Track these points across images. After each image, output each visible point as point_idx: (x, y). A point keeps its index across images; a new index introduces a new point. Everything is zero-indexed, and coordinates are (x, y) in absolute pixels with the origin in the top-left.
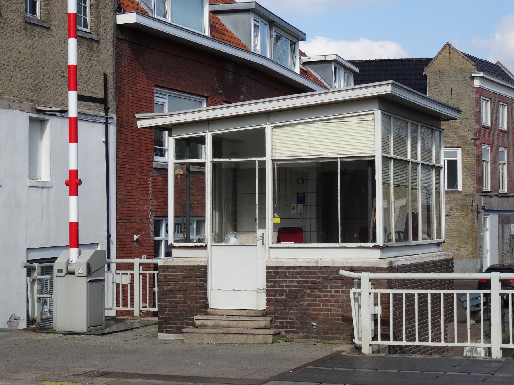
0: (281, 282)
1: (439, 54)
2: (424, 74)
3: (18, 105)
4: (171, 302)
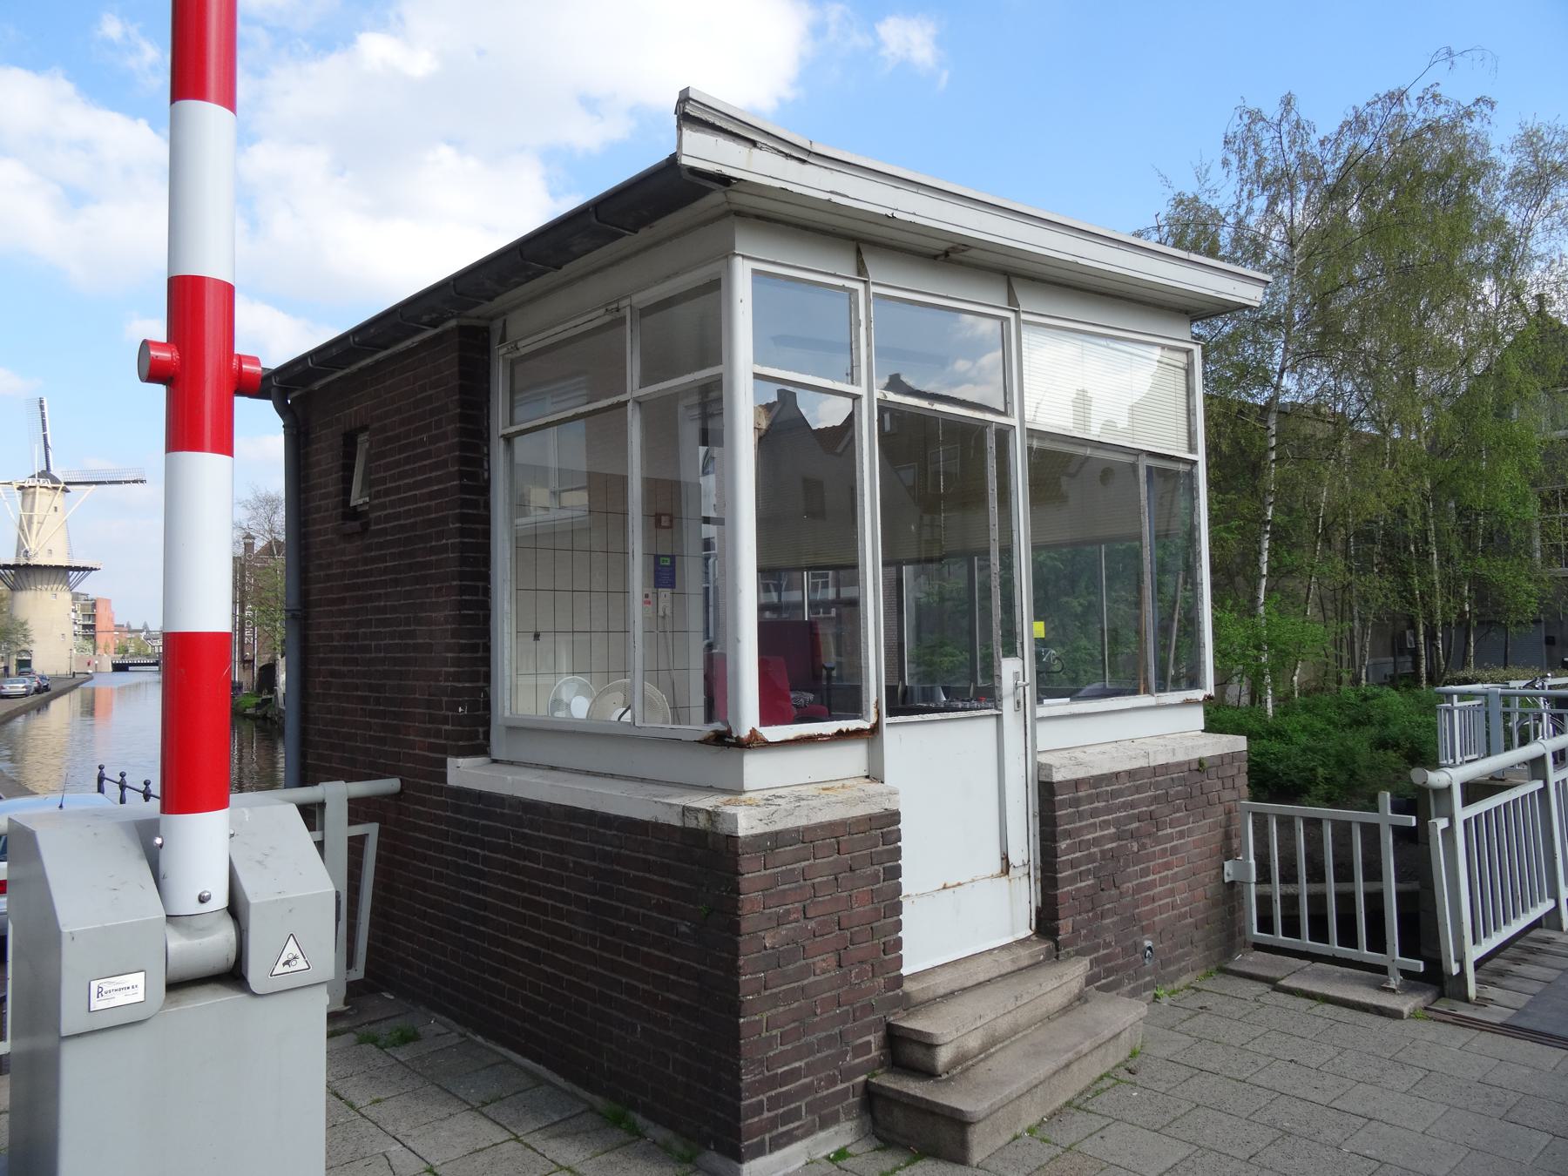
0: (1085, 832)
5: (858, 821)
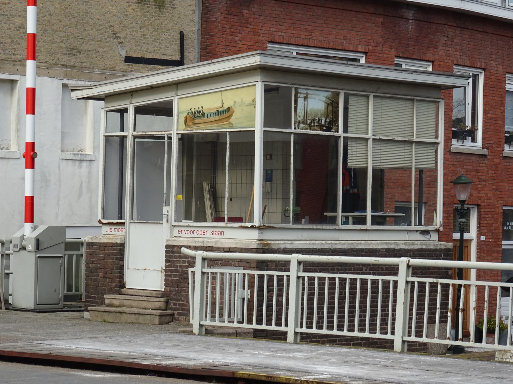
0: (176, 262)
3: (47, 71)
5: (110, 243)
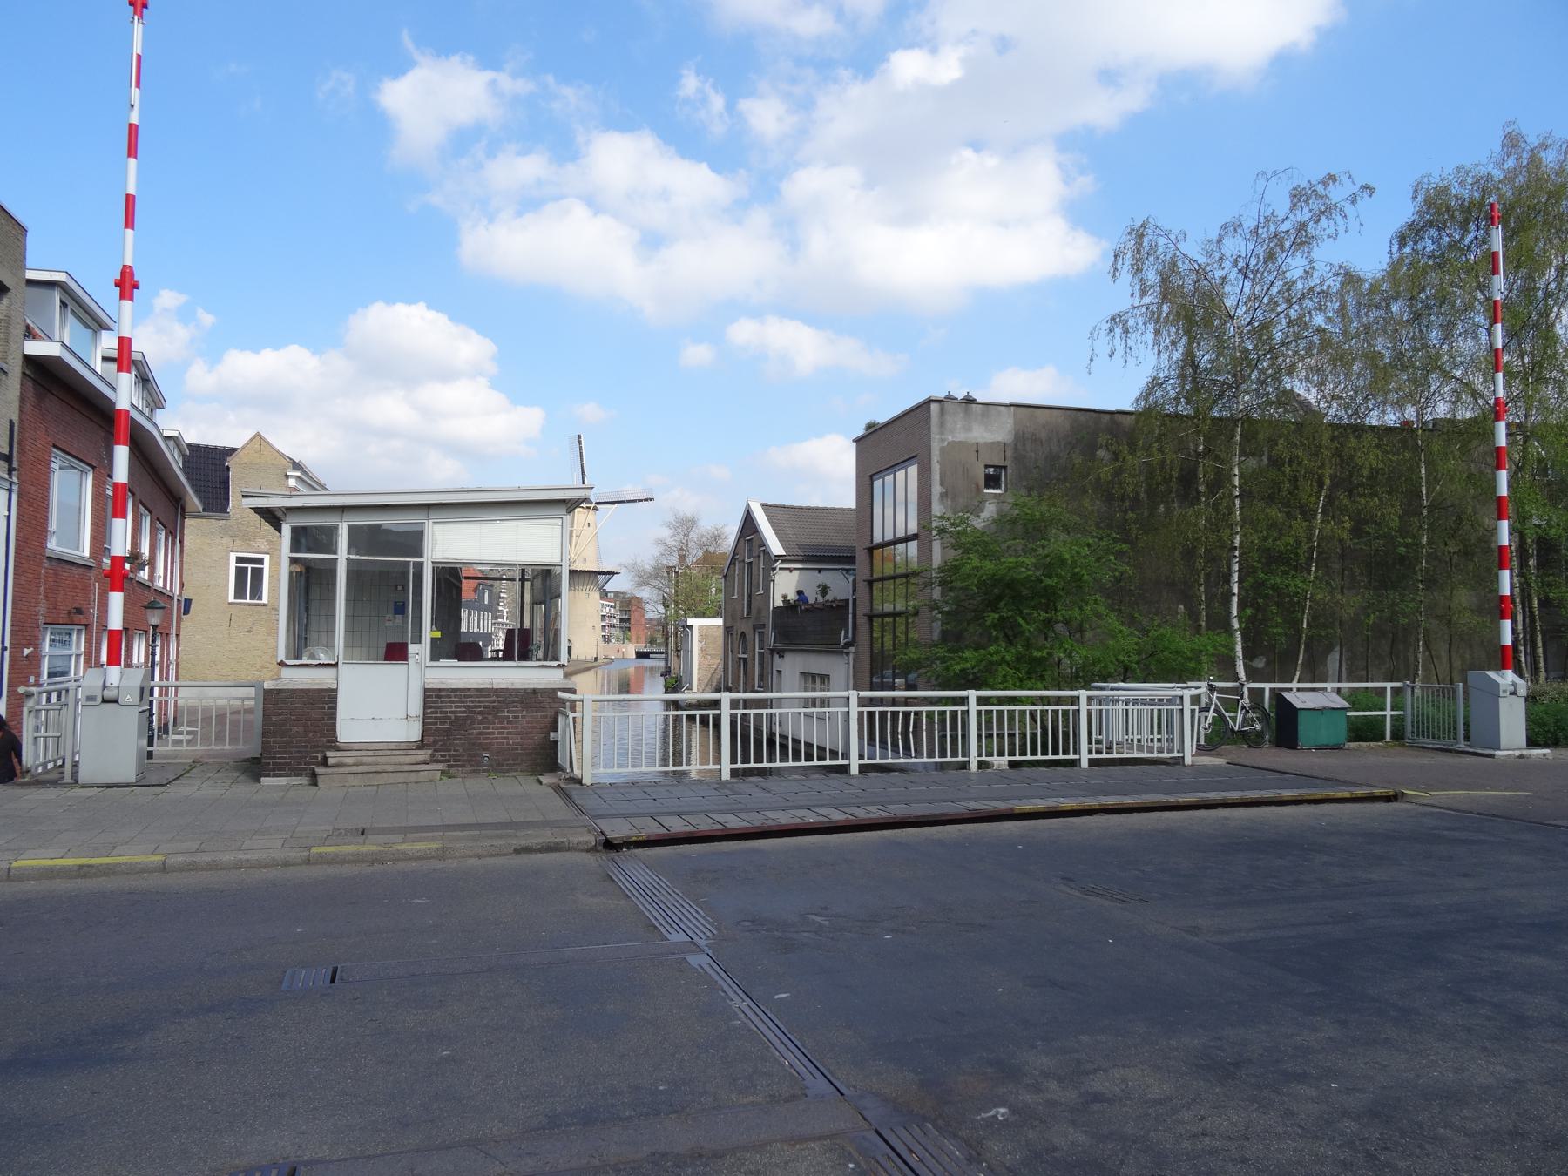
1: (247, 444)
2: (227, 464)
4: (282, 736)
